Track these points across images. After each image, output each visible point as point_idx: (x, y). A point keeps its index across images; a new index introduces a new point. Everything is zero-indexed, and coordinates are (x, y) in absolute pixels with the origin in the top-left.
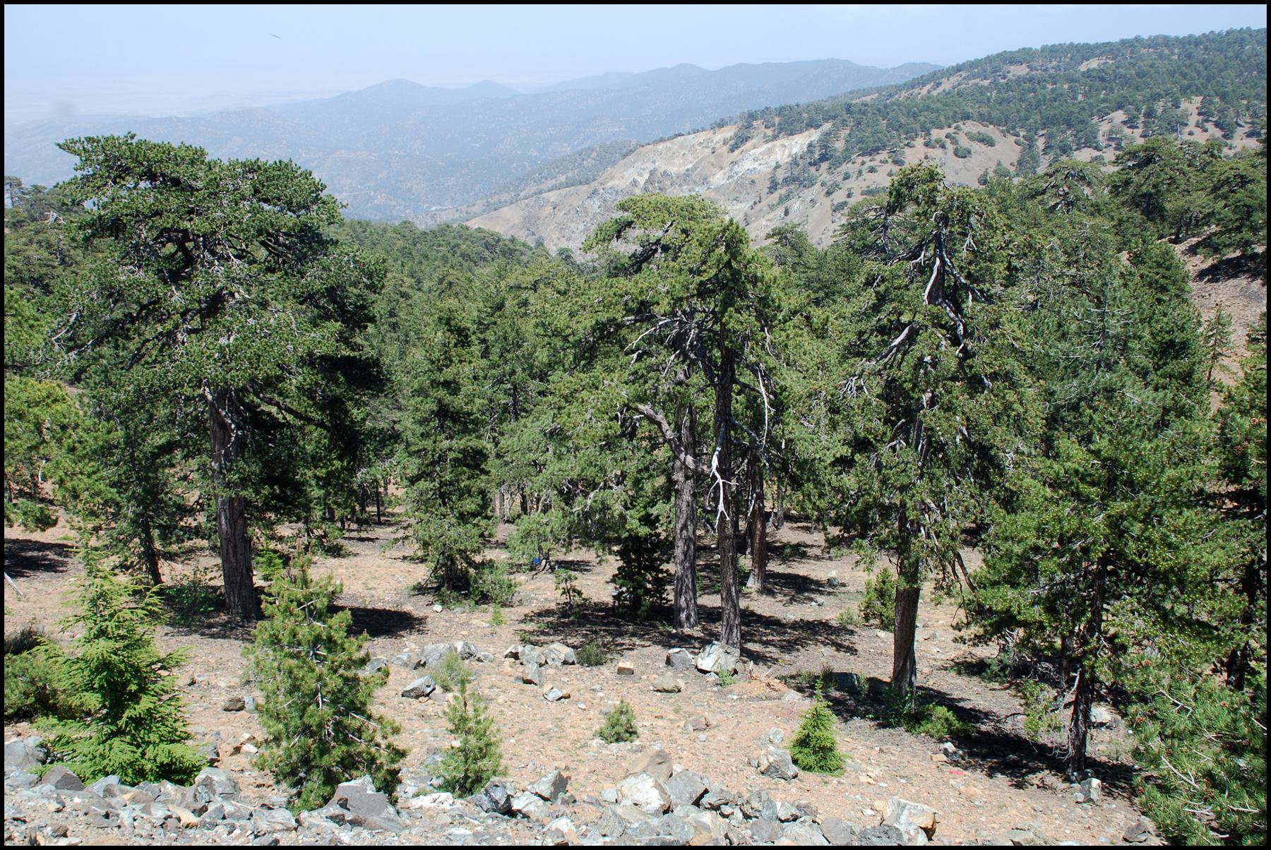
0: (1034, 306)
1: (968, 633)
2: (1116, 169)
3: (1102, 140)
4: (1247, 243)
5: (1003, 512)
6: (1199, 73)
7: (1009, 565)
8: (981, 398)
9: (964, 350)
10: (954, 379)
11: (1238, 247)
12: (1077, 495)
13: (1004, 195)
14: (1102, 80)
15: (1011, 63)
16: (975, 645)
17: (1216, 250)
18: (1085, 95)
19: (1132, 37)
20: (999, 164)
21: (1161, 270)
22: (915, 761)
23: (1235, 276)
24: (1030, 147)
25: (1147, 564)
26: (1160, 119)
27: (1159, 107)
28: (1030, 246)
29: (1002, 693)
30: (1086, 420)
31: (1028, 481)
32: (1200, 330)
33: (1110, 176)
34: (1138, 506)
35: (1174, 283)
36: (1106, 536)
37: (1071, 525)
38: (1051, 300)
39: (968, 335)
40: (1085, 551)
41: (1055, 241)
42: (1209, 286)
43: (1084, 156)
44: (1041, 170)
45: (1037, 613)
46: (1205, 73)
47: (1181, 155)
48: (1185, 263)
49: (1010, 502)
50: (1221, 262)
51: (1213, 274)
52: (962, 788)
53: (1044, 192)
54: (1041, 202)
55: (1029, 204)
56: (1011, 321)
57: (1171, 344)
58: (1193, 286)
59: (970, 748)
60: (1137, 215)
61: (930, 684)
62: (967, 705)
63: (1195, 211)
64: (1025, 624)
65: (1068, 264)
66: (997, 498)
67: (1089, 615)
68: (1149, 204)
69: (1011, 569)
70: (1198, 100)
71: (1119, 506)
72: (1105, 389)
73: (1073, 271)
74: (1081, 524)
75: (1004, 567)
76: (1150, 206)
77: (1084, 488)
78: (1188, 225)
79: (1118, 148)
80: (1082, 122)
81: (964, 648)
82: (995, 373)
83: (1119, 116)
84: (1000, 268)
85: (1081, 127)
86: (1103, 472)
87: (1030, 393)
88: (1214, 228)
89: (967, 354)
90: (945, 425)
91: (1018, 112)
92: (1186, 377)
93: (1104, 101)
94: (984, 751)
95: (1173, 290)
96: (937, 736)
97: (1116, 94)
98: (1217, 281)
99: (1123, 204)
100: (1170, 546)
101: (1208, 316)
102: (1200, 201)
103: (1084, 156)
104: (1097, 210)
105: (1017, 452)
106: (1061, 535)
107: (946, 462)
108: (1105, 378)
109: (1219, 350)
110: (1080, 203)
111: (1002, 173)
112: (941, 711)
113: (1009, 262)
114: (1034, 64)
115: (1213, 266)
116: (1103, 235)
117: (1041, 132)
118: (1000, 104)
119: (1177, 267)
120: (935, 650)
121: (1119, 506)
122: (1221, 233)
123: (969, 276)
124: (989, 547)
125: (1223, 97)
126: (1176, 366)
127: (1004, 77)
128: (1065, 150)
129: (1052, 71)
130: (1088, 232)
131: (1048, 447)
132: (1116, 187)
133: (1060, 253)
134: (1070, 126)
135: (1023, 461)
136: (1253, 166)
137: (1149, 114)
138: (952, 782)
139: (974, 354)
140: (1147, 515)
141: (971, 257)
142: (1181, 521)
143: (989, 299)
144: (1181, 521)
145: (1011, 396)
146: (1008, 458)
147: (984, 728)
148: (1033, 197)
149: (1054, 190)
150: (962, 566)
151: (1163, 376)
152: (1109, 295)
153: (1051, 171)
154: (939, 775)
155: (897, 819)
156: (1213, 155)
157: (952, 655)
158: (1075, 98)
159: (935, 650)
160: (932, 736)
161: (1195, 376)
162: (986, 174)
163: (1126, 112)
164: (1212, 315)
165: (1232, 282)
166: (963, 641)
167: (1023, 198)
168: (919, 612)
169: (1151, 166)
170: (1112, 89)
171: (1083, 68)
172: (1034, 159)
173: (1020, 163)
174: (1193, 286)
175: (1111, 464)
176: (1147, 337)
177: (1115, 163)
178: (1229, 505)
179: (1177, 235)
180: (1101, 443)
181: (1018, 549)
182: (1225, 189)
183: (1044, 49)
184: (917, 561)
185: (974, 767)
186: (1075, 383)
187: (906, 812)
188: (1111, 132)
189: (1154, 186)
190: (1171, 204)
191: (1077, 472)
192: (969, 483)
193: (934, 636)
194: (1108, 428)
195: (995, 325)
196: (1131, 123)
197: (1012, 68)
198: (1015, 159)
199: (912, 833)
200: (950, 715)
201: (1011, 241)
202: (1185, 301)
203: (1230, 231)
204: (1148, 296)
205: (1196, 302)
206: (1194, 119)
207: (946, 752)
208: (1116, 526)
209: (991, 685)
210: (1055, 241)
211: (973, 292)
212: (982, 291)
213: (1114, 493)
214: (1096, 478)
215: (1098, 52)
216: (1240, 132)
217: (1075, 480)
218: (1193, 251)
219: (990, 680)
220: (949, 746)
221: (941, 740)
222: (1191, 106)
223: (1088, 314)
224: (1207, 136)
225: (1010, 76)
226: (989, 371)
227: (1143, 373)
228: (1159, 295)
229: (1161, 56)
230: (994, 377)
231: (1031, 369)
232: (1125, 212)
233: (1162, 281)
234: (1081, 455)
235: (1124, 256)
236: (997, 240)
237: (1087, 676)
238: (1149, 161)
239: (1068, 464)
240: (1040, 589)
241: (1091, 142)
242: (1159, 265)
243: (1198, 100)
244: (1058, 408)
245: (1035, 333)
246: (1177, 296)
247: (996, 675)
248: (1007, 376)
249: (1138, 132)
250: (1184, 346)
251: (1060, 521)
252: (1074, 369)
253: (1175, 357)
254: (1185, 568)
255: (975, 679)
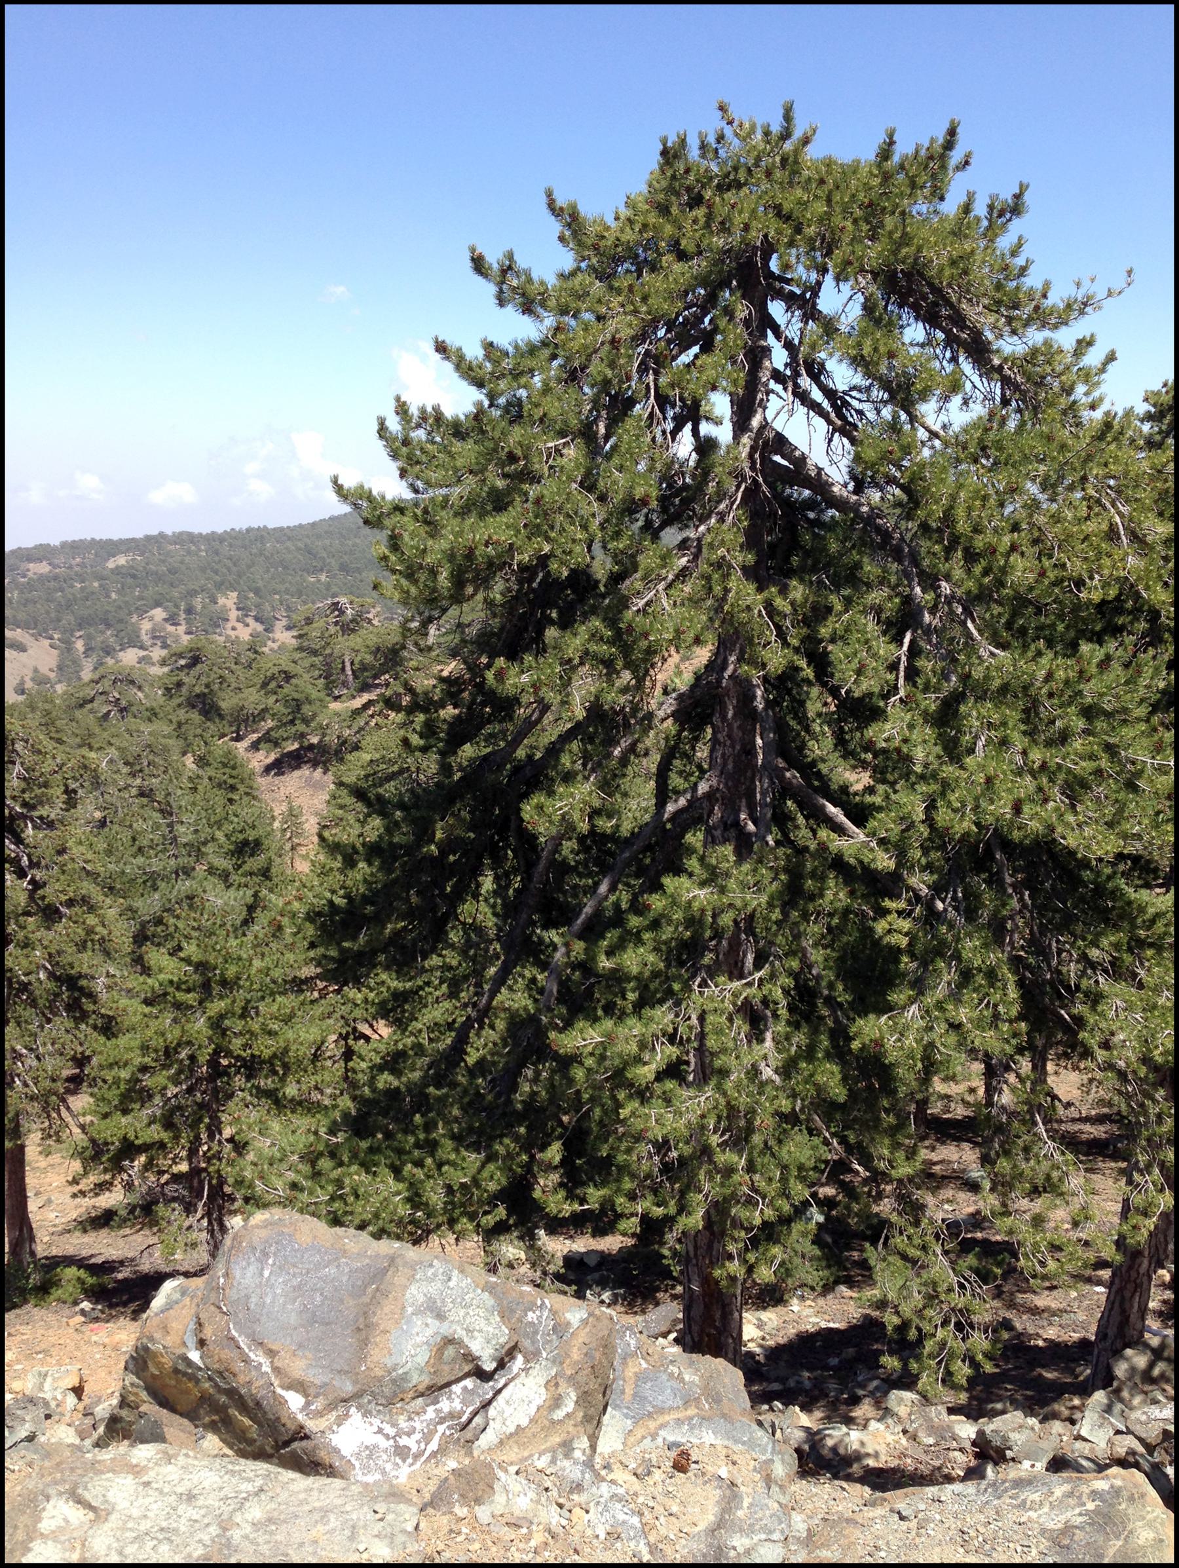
0: (102, 823)
1: (87, 1183)
2: (166, 669)
3: (145, 639)
4: (302, 736)
5: (102, 1039)
6: (229, 570)
7: (118, 1092)
8: (59, 927)
9: (33, 881)
10: (27, 914)
11: (295, 739)
12: (178, 1006)
13: (48, 706)
14: (134, 576)
15: (30, 559)
16: (97, 1195)
17: (276, 744)
18: (118, 592)
19: (155, 533)
20: (36, 670)
21: (227, 770)
22: (51, 1332)
23: (298, 767)
24: (69, 650)
25: (253, 1056)
26: (200, 614)
27: (198, 602)
28: (85, 767)
29: (134, 1237)
30: (172, 929)
31: (124, 1002)
32: (276, 825)
33: (160, 678)
34: (234, 1002)
35: (242, 781)
36: (210, 1039)
37: (173, 1035)
38: (121, 815)
39: (32, 865)
40: (192, 1058)
41: (113, 752)
42: (277, 780)
43: (130, 657)
44: (87, 675)
45: (156, 1133)
46: (234, 569)
47: (226, 654)
48: (249, 760)
49: (108, 1028)
50: (283, 755)
51: (278, 767)
52: (107, 1341)
53: (92, 700)
54: (91, 711)
55: (78, 714)
56: (81, 843)
57: (245, 843)
58: (262, 782)
59: (110, 1301)
60: (195, 716)
61: (55, 1251)
62: (99, 1260)
63: (251, 709)
64: (145, 1148)
65: (133, 775)
66: (95, 1027)
67: (207, 1120)
68: (204, 704)
69: (122, 1095)
70: (234, 595)
71: (217, 1006)
72: (188, 897)
73: (138, 781)
74: (183, 1031)
75: (113, 1095)
76: (206, 705)
77: (181, 996)
78: (246, 721)
79: (165, 646)
80: (121, 621)
81: (87, 1202)
82: (70, 900)
83: (159, 614)
84: (57, 792)
85: (120, 626)
86: (196, 977)
87: (112, 913)
88: (270, 723)
89: (36, 885)
90: (25, 963)
91: (48, 613)
92: (265, 873)
93: (141, 598)
94: (125, 1298)
95: (242, 788)
96: (71, 1300)
97: (151, 591)
98: (283, 774)
99: (179, 705)
100: (270, 1033)
101: (279, 809)
102: (253, 699)
103: (130, 657)
104: (153, 714)
105: (108, 975)
106: (167, 1048)
107: (33, 1003)
108: (185, 886)
109: (296, 841)
110: (134, 709)
111: (41, 680)
112: (71, 1272)
113: (66, 786)
114: (56, 561)
115: (276, 760)
116: (163, 741)
117: (78, 634)
118: (25, 605)
119: (242, 766)
120: (52, 1215)
121: (217, 1006)
122: (278, 727)
123: (25, 804)
124: (94, 1079)
125: (257, 592)
126: (253, 864)
127: (24, 576)
128: (108, 651)
129: (77, 569)
130: (146, 738)
131: (140, 964)
132: (168, 690)
133: (121, 765)
134: (108, 626)
135: (116, 984)
136: (294, 662)
137: (189, 611)
138: (94, 1338)
139: (45, 884)
140: (245, 1009)
141: (23, 785)
142: (275, 1007)
143: (51, 825)
144: (275, 1007)
145: (91, 920)
146: (100, 984)
147: (120, 1276)
148: (81, 706)
149: (103, 697)
150: (68, 1108)
151: (244, 875)
152: (174, 805)
153: (96, 677)
154: (78, 1337)
155: (41, 1389)
156: (256, 652)
157: (74, 1215)
158: (108, 596)
159: (52, 1215)
160: (64, 1302)
161: (273, 870)
162: (22, 682)
163: (166, 609)
164: (284, 807)
165: (297, 773)
166: (83, 1193)
167: (70, 708)
168: (27, 1180)
169: (199, 666)
170: (146, 587)
171: (111, 564)
172: (76, 662)
173: (60, 668)
174: (262, 782)
175: (202, 967)
176: (223, 839)
177: (163, 663)
178: (321, 984)
179: (237, 732)
180: (191, 949)
181: (125, 1074)
182: (273, 685)
183: (64, 545)
184: (17, 1115)
185: (116, 1317)
186: (157, 896)
187: (49, 1379)
188: (153, 630)
189: (207, 686)
190: (227, 703)
191: (171, 982)
192: (62, 1022)
193: (49, 1201)
194: (195, 934)
195: (61, 851)
196: (172, 620)
197: (31, 566)
198: (53, 664)
199: (59, 1397)
200: (82, 1273)
201: (63, 764)
202: (254, 798)
203: (285, 725)
204: (218, 798)
205: (266, 797)
206: (234, 614)
207: (83, 1312)
208: (217, 1024)
209: (122, 1232)
210: (113, 752)
211: (32, 821)
212: (41, 818)
213: (210, 995)
214: (191, 984)
215: (123, 548)
216: (280, 625)
217: (171, 990)
218: (255, 746)
219: (120, 1227)
220: (86, 1305)
221: (76, 1303)
222: (228, 601)
223: (157, 826)
224: (249, 630)
225: (30, 574)
226: (64, 898)
227: (225, 876)
228: (230, 795)
229: (189, 552)
230: (70, 903)
231: (111, 889)
232: (182, 714)
233: (231, 781)
234: (172, 965)
235: (189, 760)
236: (48, 766)
237: (214, 1182)
238: (195, 661)
239: (161, 977)
240: (155, 1107)
241: (134, 641)
242: (225, 765)
243: (234, 595)
244: (143, 925)
245: (109, 852)
246: (247, 794)
247: (125, 1220)
248: (85, 900)
249: (181, 629)
250: (258, 843)
251: (163, 1034)
252: (152, 881)
253: (252, 855)
254: (286, 1050)
255: (104, 1232)
